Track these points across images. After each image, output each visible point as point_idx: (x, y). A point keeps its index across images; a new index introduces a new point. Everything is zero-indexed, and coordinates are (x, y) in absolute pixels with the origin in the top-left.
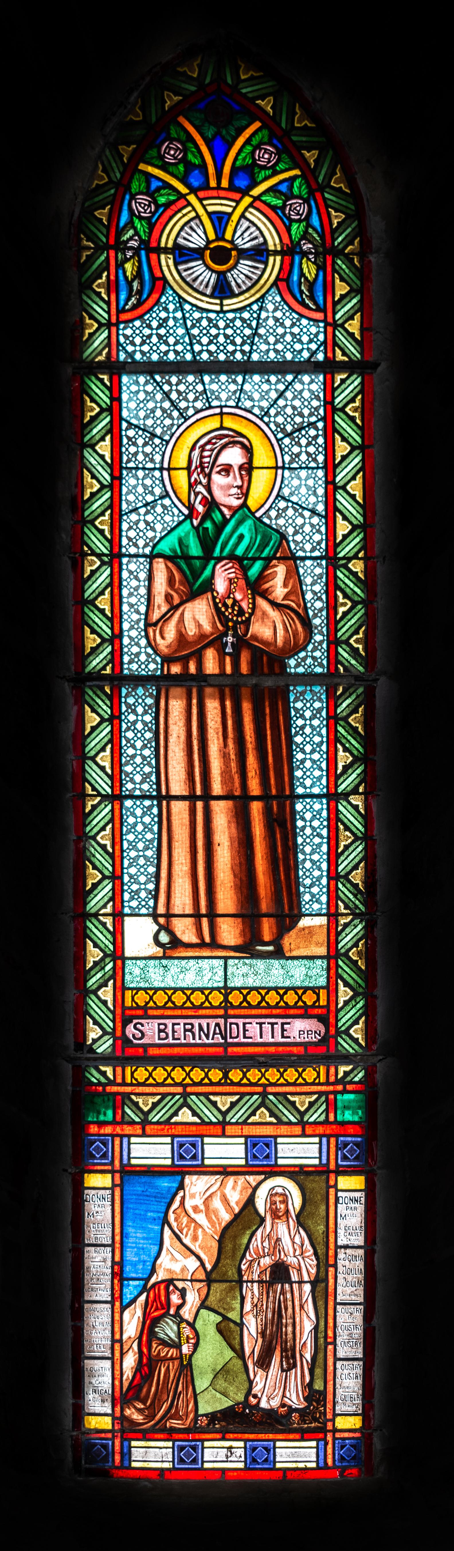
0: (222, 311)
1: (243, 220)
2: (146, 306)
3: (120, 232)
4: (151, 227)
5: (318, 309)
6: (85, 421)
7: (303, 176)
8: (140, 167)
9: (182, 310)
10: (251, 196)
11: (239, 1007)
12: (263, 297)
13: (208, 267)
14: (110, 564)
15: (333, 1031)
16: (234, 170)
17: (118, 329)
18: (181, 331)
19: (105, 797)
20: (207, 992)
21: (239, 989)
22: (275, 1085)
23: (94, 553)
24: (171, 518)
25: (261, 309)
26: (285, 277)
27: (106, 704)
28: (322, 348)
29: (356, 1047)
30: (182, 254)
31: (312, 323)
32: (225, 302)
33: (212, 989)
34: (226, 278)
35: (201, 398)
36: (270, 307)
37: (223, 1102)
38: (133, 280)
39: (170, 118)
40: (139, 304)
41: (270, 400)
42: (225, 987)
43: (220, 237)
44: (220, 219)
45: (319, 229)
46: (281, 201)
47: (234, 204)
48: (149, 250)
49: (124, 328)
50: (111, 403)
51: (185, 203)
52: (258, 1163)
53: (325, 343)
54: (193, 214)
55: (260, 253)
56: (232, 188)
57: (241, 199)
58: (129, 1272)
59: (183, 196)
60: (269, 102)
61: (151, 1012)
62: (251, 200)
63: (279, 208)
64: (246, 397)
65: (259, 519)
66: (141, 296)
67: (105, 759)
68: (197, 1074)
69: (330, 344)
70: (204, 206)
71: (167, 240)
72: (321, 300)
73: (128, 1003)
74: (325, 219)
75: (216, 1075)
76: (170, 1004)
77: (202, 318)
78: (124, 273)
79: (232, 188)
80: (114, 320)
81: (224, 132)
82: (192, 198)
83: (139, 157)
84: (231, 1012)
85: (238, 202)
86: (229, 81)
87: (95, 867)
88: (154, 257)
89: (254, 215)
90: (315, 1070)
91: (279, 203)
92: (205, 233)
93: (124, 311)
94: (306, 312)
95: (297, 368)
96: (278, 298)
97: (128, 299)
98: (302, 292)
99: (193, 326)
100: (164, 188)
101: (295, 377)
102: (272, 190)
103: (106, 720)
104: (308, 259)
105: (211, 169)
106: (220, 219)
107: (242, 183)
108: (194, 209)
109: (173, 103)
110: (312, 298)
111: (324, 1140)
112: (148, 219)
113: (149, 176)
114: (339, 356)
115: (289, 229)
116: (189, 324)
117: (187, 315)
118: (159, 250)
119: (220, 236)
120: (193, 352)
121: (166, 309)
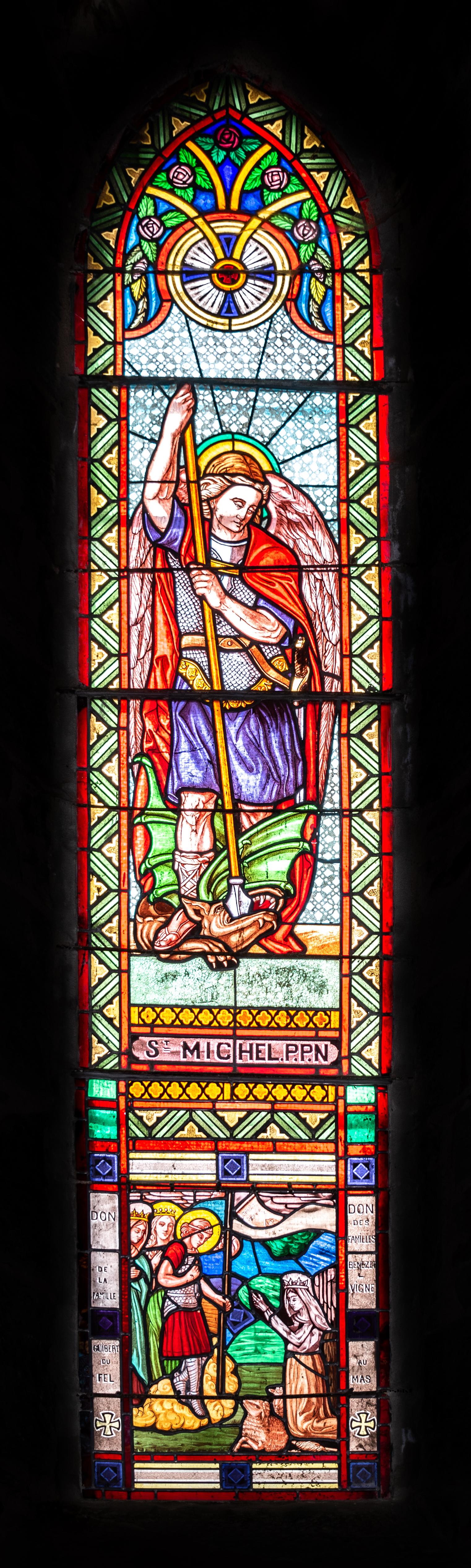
0: (230, 331)
2: (154, 324)
3: (127, 256)
4: (159, 248)
5: (327, 332)
7: (313, 198)
8: (147, 192)
10: (260, 218)
11: (248, 1028)
12: (271, 317)
13: (215, 286)
14: (119, 579)
15: (345, 1053)
16: (244, 193)
19: (111, 809)
21: (249, 1008)
23: (100, 569)
30: (189, 274)
31: (320, 345)
36: (279, 328)
38: (140, 300)
39: (178, 144)
40: (146, 322)
44: (228, 241)
45: (328, 249)
47: (242, 225)
48: (156, 273)
51: (193, 225)
53: (334, 364)
54: (200, 236)
55: (268, 273)
59: (190, 219)
60: (278, 126)
61: (157, 1030)
62: (259, 222)
63: (288, 231)
67: (112, 462)
70: (212, 229)
71: (174, 262)
73: (135, 1019)
78: (132, 294)
80: (119, 339)
81: (232, 155)
82: (199, 221)
84: (239, 1032)
85: (246, 223)
87: (100, 1041)
88: (161, 278)
89: (262, 236)
92: (214, 252)
93: (129, 330)
96: (287, 319)
97: (136, 315)
98: (310, 315)
100: (172, 211)
102: (282, 212)
103: (114, 501)
106: (228, 241)
108: (201, 230)
110: (321, 317)
115: (297, 251)
119: (228, 255)
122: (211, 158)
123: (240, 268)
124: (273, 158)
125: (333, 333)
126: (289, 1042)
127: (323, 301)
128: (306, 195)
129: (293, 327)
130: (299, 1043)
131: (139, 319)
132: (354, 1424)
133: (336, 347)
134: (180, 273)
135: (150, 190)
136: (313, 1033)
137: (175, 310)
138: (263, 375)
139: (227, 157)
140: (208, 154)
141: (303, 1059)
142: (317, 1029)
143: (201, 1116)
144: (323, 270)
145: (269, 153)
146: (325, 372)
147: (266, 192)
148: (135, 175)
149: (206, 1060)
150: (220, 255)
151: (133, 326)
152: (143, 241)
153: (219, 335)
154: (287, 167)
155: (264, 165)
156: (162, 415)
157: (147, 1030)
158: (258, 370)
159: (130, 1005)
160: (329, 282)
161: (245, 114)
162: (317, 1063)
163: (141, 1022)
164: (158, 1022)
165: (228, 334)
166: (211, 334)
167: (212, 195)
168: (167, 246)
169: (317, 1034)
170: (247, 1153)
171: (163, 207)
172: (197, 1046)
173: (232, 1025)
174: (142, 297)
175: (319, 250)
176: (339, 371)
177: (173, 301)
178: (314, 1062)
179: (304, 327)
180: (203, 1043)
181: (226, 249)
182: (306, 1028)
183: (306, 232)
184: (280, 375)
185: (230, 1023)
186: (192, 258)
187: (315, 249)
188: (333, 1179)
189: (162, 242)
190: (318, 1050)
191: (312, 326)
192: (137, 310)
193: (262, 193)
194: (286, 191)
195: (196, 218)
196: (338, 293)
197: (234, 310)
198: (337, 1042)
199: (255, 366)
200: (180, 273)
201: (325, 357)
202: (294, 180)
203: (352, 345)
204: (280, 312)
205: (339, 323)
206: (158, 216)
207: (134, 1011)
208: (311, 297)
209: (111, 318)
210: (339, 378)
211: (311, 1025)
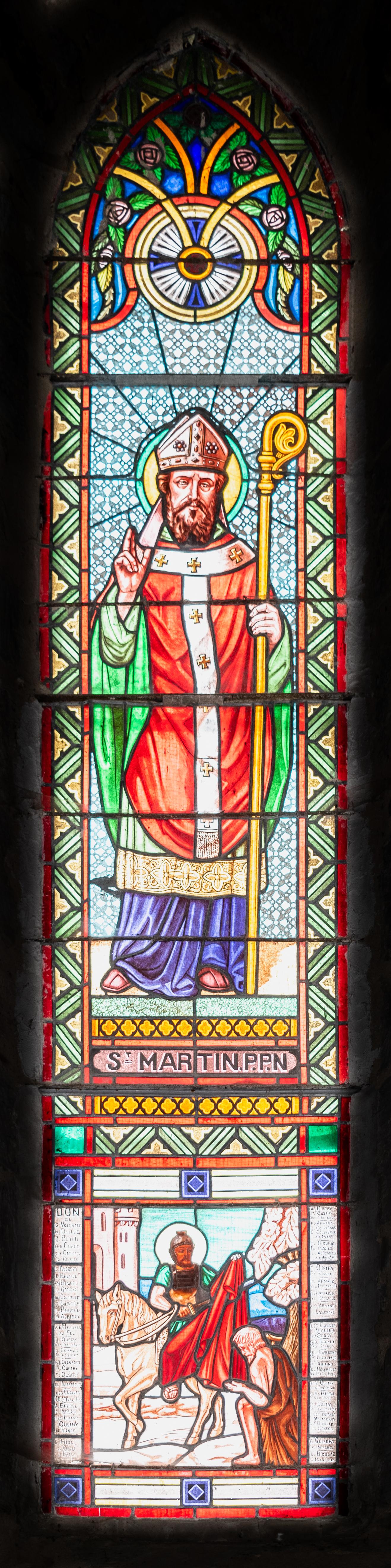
0: (195, 323)
1: (219, 228)
6: (55, 440)
7: (282, 183)
9: (155, 321)
12: (238, 309)
13: (182, 276)
16: (213, 175)
21: (209, 1019)
24: (274, 402)
26: (261, 288)
27: (76, 729)
28: (297, 362)
29: (328, 1080)
30: (157, 261)
32: (199, 313)
34: (200, 287)
35: (114, 510)
37: (198, 1134)
40: (112, 315)
41: (241, 414)
43: (196, 244)
44: (196, 225)
47: (212, 210)
53: (300, 356)
54: (168, 220)
55: (235, 262)
56: (210, 194)
57: (219, 205)
58: (78, 1150)
59: (159, 202)
64: (218, 410)
66: (113, 307)
69: (306, 356)
70: (180, 212)
77: (175, 330)
78: (98, 283)
79: (210, 194)
80: (85, 332)
82: (168, 205)
83: (114, 160)
85: (216, 208)
88: (128, 268)
89: (231, 224)
91: (256, 211)
97: (103, 306)
98: (277, 303)
99: (167, 338)
101: (268, 392)
104: (285, 268)
106: (196, 225)
107: (221, 187)
108: (169, 215)
109: (150, 105)
113: (123, 180)
114: (316, 370)
116: (162, 336)
117: (160, 327)
118: (133, 261)
123: (207, 256)
124: (242, 139)
127: (292, 290)
129: (261, 320)
131: (106, 311)
134: (148, 261)
135: (118, 171)
142: (276, 1038)
144: (290, 260)
145: (237, 133)
146: (290, 366)
148: (103, 153)
150: (188, 242)
153: (186, 327)
154: (256, 148)
155: (233, 147)
156: (121, 538)
158: (223, 366)
159: (91, 1017)
160: (298, 270)
162: (276, 1071)
166: (178, 327)
168: (134, 233)
170: (210, 1169)
171: (130, 189)
172: (154, 1058)
174: (108, 289)
175: (287, 240)
177: (140, 293)
178: (273, 1071)
180: (161, 1055)
181: (194, 232)
182: (265, 1037)
183: (273, 220)
186: (159, 245)
187: (284, 238)
189: (129, 226)
190: (277, 1059)
195: (164, 200)
197: (201, 301)
198: (295, 1051)
199: (220, 361)
200: (148, 261)
201: (291, 351)
206: (125, 199)
209: (77, 559)
211: (271, 1034)
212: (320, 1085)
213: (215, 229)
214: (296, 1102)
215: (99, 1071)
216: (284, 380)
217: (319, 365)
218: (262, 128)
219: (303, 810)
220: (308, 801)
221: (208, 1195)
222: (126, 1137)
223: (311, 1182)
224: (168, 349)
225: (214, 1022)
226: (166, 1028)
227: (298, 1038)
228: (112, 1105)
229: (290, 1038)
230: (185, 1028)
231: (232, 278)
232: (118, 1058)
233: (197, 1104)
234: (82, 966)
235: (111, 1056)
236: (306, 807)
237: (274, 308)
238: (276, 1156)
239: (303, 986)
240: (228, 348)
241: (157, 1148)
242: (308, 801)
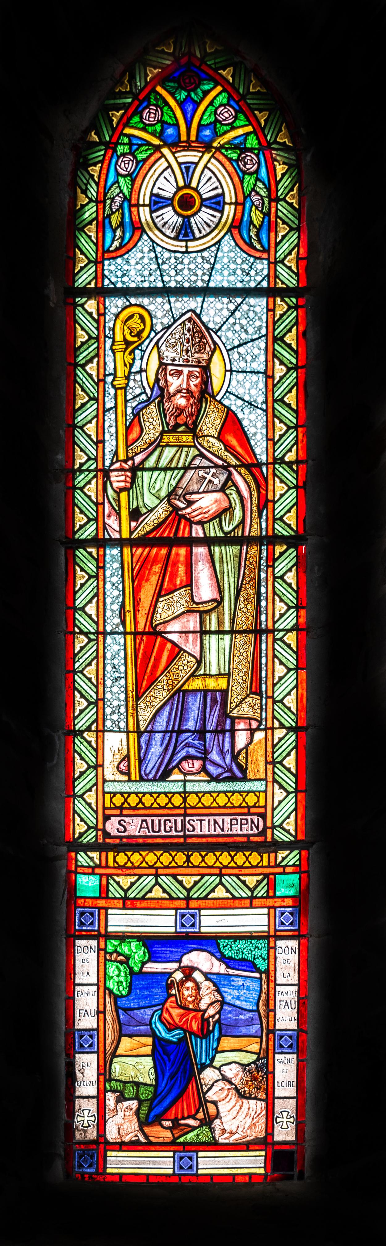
0: (187, 252)
1: (206, 170)
4: (133, 181)
9: (155, 252)
12: (219, 242)
16: (200, 127)
17: (103, 265)
18: (154, 266)
20: (170, 795)
22: (226, 867)
23: (82, 632)
25: (218, 250)
33: (174, 793)
37: (188, 881)
38: (117, 228)
42: (185, 792)
44: (188, 169)
46: (236, 155)
49: (109, 265)
50: (97, 571)
52: (285, 928)
53: (268, 275)
61: (125, 812)
65: (220, 402)
66: (122, 241)
68: (166, 858)
69: (273, 275)
70: (176, 158)
72: (265, 241)
73: (108, 804)
74: (271, 170)
75: (180, 858)
76: (140, 805)
78: (110, 223)
81: (193, 95)
84: (189, 811)
86: (198, 55)
89: (214, 165)
90: (259, 854)
94: (253, 252)
95: (246, 292)
97: (113, 240)
98: (250, 237)
99: (164, 263)
105: (182, 122)
110: (259, 241)
111: (272, 911)
112: (130, 175)
117: (159, 255)
120: (163, 281)
121: (142, 251)
122: (175, 98)
125: (268, 251)
126: (231, 817)
127: (261, 226)
128: (250, 129)
129: (237, 248)
130: (239, 818)
131: (116, 244)
132: (279, 1120)
133: (269, 263)
135: (127, 131)
136: (246, 810)
137: (145, 237)
138: (212, 285)
139: (188, 96)
140: (172, 95)
141: (241, 830)
142: (249, 807)
143: (165, 880)
145: (220, 93)
147: (218, 125)
149: (213, 833)
151: (111, 249)
152: (120, 178)
155: (217, 103)
157: (118, 812)
161: (203, 61)
163: (112, 806)
164: (126, 805)
165: (186, 255)
167: (176, 127)
169: (249, 811)
170: (199, 909)
173: (183, 806)
176: (272, 279)
179: (245, 248)
184: (226, 285)
185: (181, 804)
188: (266, 929)
189: (134, 175)
190: (252, 822)
191: (251, 245)
192: (115, 236)
193: (216, 125)
194: (234, 125)
196: (273, 219)
198: (263, 816)
202: (242, 117)
203: (282, 262)
204: (227, 237)
205: (272, 245)
207: (108, 797)
208: (251, 222)
210: (272, 285)
212: (284, 841)
213: (202, 172)
214: (265, 856)
215: (109, 834)
216: (257, 292)
217: (283, 283)
218: (241, 91)
219: (271, 628)
220: (274, 623)
221: (197, 930)
222: (132, 884)
223: (277, 919)
224: (165, 271)
225: (200, 795)
226: (162, 800)
227: (265, 807)
228: (122, 859)
229: (259, 807)
230: (177, 800)
231: (215, 217)
232: (125, 824)
233: (188, 857)
234: (96, 750)
235: (120, 823)
236: (274, 626)
237: (247, 240)
238: (252, 898)
239: (270, 767)
240: (212, 268)
241: (158, 893)
242: (274, 623)
